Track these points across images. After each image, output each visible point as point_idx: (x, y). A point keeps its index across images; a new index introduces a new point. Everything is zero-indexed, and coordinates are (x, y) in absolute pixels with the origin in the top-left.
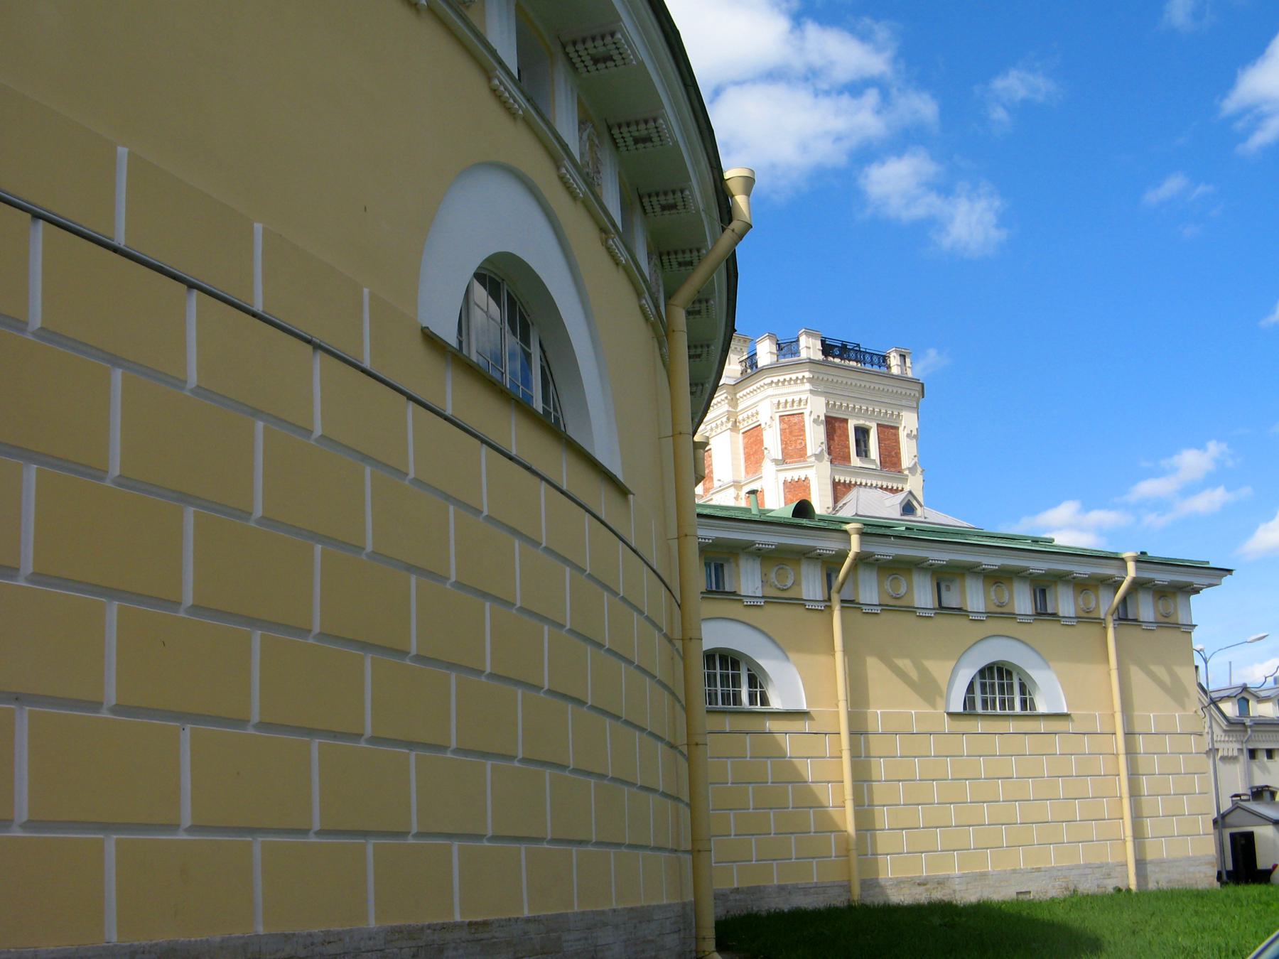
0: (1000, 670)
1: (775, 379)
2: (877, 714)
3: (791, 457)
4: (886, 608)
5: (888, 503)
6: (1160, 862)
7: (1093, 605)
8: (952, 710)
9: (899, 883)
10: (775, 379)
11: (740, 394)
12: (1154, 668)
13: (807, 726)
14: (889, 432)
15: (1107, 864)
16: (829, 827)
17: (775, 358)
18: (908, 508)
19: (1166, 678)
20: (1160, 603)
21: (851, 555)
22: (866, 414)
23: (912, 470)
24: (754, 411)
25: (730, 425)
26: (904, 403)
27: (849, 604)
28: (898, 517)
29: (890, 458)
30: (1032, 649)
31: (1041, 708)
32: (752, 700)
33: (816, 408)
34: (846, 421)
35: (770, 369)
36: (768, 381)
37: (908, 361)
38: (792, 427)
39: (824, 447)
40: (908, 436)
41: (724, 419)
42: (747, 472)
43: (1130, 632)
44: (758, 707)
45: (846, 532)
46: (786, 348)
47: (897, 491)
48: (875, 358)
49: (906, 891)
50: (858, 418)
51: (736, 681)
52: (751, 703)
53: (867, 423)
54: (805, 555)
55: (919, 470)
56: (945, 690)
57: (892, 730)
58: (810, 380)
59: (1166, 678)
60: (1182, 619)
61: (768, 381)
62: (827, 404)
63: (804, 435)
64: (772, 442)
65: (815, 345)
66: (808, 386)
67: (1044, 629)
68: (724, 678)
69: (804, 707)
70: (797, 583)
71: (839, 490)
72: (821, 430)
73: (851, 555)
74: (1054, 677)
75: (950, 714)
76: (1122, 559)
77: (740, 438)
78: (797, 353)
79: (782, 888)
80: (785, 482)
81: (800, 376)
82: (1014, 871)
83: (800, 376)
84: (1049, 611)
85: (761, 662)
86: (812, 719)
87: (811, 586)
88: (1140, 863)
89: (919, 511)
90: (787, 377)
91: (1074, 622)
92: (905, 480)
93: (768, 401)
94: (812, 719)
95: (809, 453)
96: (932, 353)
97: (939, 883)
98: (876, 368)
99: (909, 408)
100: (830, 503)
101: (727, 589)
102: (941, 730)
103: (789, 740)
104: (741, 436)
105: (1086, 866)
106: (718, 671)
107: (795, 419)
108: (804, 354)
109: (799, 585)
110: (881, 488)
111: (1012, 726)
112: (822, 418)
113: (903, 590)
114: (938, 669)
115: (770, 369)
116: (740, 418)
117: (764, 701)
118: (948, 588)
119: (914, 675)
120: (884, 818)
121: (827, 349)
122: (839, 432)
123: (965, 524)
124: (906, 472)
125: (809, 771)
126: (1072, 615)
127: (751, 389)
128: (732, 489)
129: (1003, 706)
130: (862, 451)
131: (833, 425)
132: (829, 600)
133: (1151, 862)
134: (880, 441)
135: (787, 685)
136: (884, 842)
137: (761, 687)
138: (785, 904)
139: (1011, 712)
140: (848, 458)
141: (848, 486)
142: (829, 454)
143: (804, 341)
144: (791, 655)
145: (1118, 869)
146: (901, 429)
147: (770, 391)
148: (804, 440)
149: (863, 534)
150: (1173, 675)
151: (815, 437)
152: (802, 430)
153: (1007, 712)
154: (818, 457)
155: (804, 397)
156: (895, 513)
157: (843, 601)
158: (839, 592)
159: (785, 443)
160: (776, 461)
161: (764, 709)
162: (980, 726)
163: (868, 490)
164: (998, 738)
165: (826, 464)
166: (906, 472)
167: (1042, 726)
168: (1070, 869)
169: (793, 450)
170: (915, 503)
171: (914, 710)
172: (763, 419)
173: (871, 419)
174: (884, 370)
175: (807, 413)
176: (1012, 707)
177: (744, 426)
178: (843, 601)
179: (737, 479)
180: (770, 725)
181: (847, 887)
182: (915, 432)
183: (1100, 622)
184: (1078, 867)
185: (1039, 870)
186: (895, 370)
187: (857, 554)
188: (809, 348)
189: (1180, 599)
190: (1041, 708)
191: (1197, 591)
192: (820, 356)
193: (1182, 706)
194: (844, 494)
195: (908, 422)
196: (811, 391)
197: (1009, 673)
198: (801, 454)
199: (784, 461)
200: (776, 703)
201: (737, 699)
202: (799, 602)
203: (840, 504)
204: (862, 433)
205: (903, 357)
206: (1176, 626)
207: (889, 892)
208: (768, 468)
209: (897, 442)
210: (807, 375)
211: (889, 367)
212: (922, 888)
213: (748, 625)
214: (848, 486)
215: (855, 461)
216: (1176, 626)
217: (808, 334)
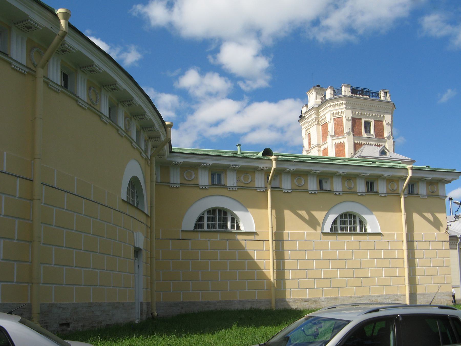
0: (350, 215)
1: (332, 104)
2: (288, 233)
3: (338, 134)
4: (293, 190)
5: (375, 151)
6: (423, 295)
7: (352, 186)
8: (324, 231)
9: (295, 301)
10: (332, 104)
11: (320, 111)
12: (300, 212)
13: (255, 237)
14: (379, 124)
15: (397, 295)
16: (263, 276)
17: (332, 96)
18: (383, 153)
19: (431, 218)
20: (430, 187)
21: (273, 169)
22: (369, 117)
23: (389, 138)
24: (325, 117)
25: (316, 123)
26: (385, 111)
27: (274, 189)
28: (379, 156)
29: (379, 133)
31: (369, 231)
32: (232, 227)
33: (347, 114)
34: (361, 119)
35: (330, 100)
36: (329, 105)
37: (388, 95)
38: (338, 122)
39: (351, 129)
40: (387, 124)
41: (314, 121)
42: (323, 141)
43: (413, 199)
44: (235, 230)
45: (271, 160)
46: (337, 92)
47: (380, 146)
48: (374, 94)
49: (299, 304)
50: (366, 117)
51: (226, 220)
52: (360, 231)
53: (370, 120)
54: (255, 169)
55: (391, 137)
56: (321, 223)
57: (295, 239)
58: (345, 104)
59: (431, 218)
60: (441, 193)
61: (329, 105)
62: (353, 113)
63: (343, 125)
64: (331, 129)
65: (348, 90)
66: (344, 106)
67: (371, 198)
68: (220, 219)
69: (254, 230)
70: (253, 180)
71: (357, 146)
72: (350, 123)
73: (273, 169)
74: (375, 218)
75: (323, 233)
76: (407, 169)
77: (320, 127)
78: (341, 94)
79: (240, 301)
81: (341, 102)
82: (351, 297)
84: (375, 191)
86: (383, 236)
87: (259, 182)
88: (413, 295)
89: (388, 154)
90: (334, 104)
91: (386, 195)
92: (385, 142)
93: (329, 113)
94: (383, 236)
95: (345, 132)
96: (449, 91)
97: (314, 301)
98: (374, 98)
99: (388, 113)
100: (352, 151)
101: (222, 184)
102: (434, 240)
103: (247, 243)
104: (321, 127)
105: (386, 295)
106: (348, 220)
107: (340, 119)
108: (343, 94)
109: (254, 181)
110: (375, 145)
111: (354, 238)
112: (350, 118)
113: (303, 183)
114: (319, 215)
115: (330, 100)
116: (320, 120)
117: (238, 227)
118: (326, 182)
119: (307, 217)
120: (289, 274)
121: (354, 91)
122: (357, 124)
123: (408, 158)
124: (386, 139)
125: (255, 255)
126: (385, 192)
127: (323, 108)
128: (317, 148)
129: (351, 230)
130: (367, 130)
131: (355, 121)
132: (267, 188)
133: (419, 294)
134: (375, 126)
135: (247, 220)
136: (288, 284)
137: (364, 225)
138: (238, 307)
139: (355, 232)
140: (361, 134)
141: (361, 145)
142: (353, 132)
143: (343, 88)
144: (373, 212)
145: (402, 297)
146: (384, 121)
147: (330, 109)
148: (343, 127)
149: (277, 160)
150: (435, 218)
151: (347, 126)
152: (342, 123)
153: (353, 232)
154: (348, 134)
156: (378, 155)
157: (272, 188)
158: (270, 184)
159: (336, 129)
160: (332, 136)
161: (238, 231)
162: (338, 238)
163: (369, 146)
164: (346, 244)
165: (351, 137)
166: (386, 139)
167: (368, 238)
168: (379, 296)
169: (339, 132)
170: (386, 151)
171: (307, 230)
172: (328, 120)
173: (371, 119)
174: (377, 98)
175: (344, 116)
176: (355, 230)
177: (322, 123)
178: (272, 188)
179: (319, 143)
180: (238, 237)
181: (270, 301)
182: (390, 123)
183: (399, 196)
184: (382, 296)
185: (363, 296)
186: (382, 99)
187: (275, 169)
188: (346, 91)
189: (440, 186)
190: (369, 231)
191: (449, 182)
192: (350, 94)
193: (439, 230)
194: (359, 148)
195: (387, 119)
196: (346, 108)
197: (355, 217)
198: (342, 133)
199: (335, 136)
200: (243, 229)
201: (226, 226)
202: (254, 188)
203: (357, 152)
204: (367, 124)
205: (386, 93)
206: (438, 196)
207: (290, 304)
208: (329, 139)
209: (383, 127)
210: (344, 102)
211: (380, 97)
212: (306, 303)
213: (227, 196)
214: (361, 145)
215: (364, 135)
216: (438, 196)
217: (345, 86)
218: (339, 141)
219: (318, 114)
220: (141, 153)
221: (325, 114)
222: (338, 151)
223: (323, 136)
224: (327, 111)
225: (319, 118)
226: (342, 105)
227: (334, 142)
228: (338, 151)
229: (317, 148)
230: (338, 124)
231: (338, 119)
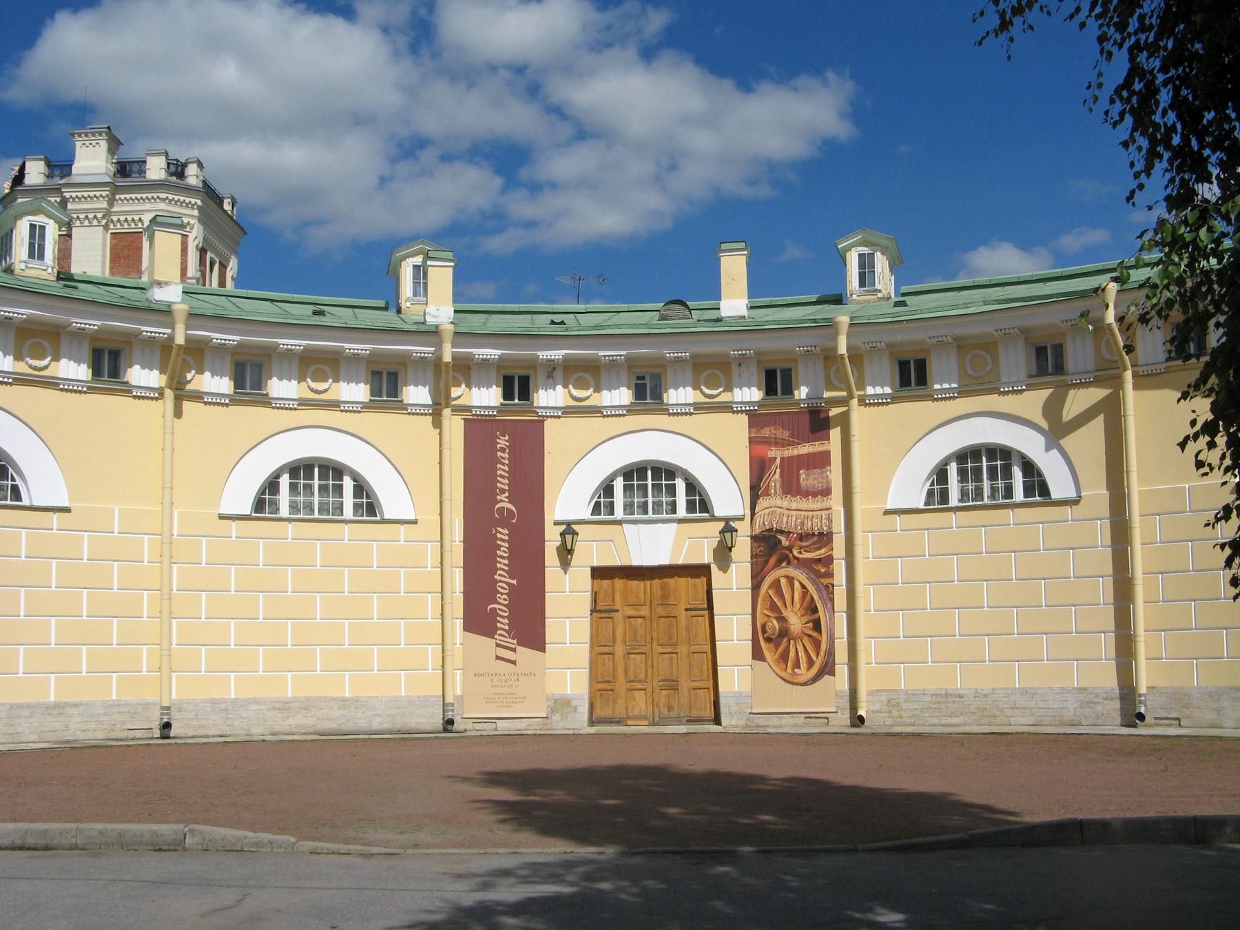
25: (104, 222)
58: (199, 208)
66: (196, 213)
81: (193, 201)
155: (192, 221)
210: (199, 203)
219: (111, 202)
223: (111, 261)
226: (192, 208)
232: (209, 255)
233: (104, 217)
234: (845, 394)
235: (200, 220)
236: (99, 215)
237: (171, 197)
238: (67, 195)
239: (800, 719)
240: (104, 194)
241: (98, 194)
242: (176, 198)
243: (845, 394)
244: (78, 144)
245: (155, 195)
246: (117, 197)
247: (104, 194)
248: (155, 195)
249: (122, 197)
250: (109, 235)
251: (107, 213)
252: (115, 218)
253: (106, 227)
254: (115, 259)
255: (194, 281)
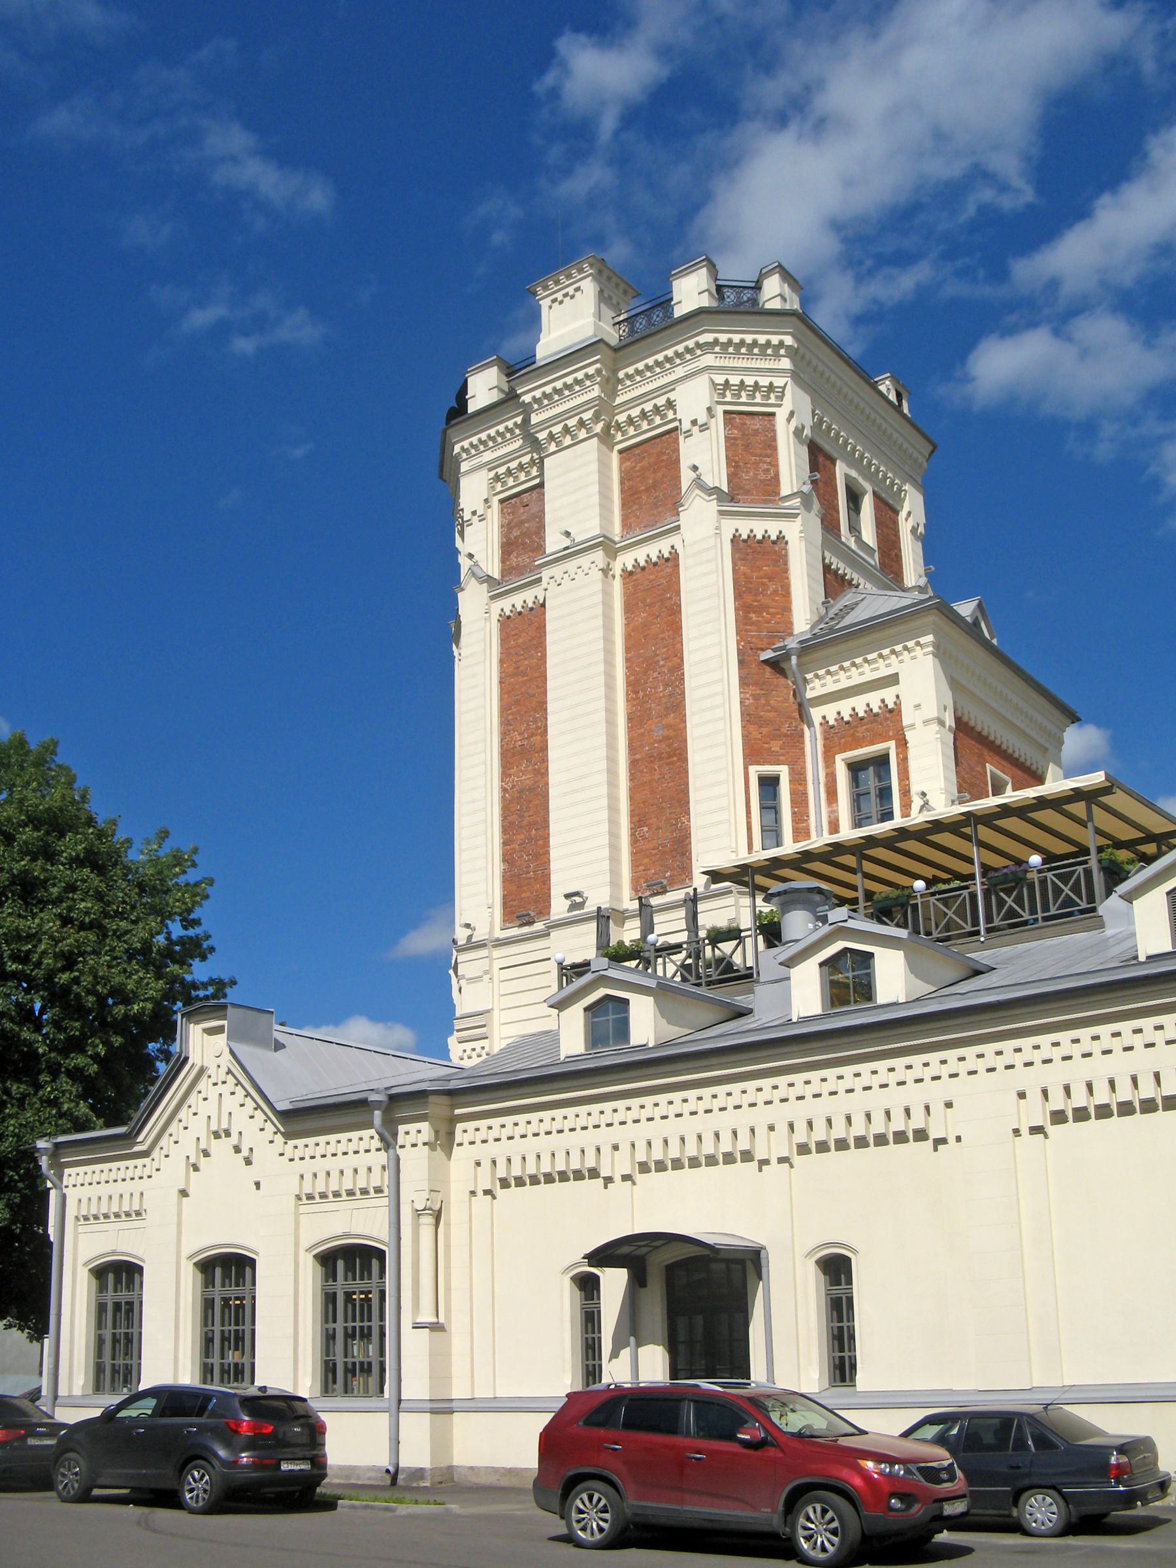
1: (723, 338)
3: (747, 492)
25: (598, 428)
30: (747, 1503)
36: (708, 337)
38: (749, 438)
58: (792, 353)
61: (708, 337)
64: (704, 456)
66: (786, 363)
80: (735, 540)
81: (775, 339)
83: (775, 339)
85: (323, 1416)
93: (703, 381)
95: (785, 490)
107: (756, 424)
128: (599, 556)
146: (903, 515)
151: (791, 468)
152: (771, 445)
155: (779, 382)
169: (750, 482)
175: (781, 414)
198: (769, 489)
199: (731, 497)
210: (789, 340)
218: (759, 528)
219: (611, 385)
220: (656, 1247)
221: (671, 386)
222: (748, 578)
223: (625, 504)
224: (680, 372)
225: (613, 411)
226: (776, 355)
227: (730, 526)
228: (748, 578)
229: (599, 556)
230: (747, 447)
231: (748, 421)
232: (841, 470)
233: (597, 418)
234: (305, 1466)
235: (795, 375)
236: (587, 416)
237: (723, 338)
238: (527, 398)
239: (428, 1084)
240: (591, 370)
241: (580, 375)
242: (736, 338)
243: (305, 1466)
244: (545, 304)
245: (691, 343)
246: (621, 375)
247: (591, 370)
248: (691, 343)
249: (630, 370)
250: (615, 457)
251: (604, 408)
252: (622, 418)
253: (606, 438)
254: (630, 498)
255: (796, 502)
